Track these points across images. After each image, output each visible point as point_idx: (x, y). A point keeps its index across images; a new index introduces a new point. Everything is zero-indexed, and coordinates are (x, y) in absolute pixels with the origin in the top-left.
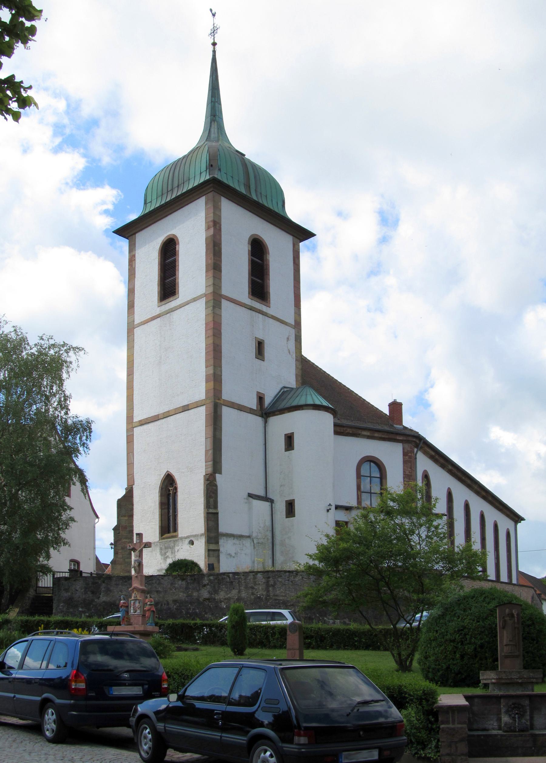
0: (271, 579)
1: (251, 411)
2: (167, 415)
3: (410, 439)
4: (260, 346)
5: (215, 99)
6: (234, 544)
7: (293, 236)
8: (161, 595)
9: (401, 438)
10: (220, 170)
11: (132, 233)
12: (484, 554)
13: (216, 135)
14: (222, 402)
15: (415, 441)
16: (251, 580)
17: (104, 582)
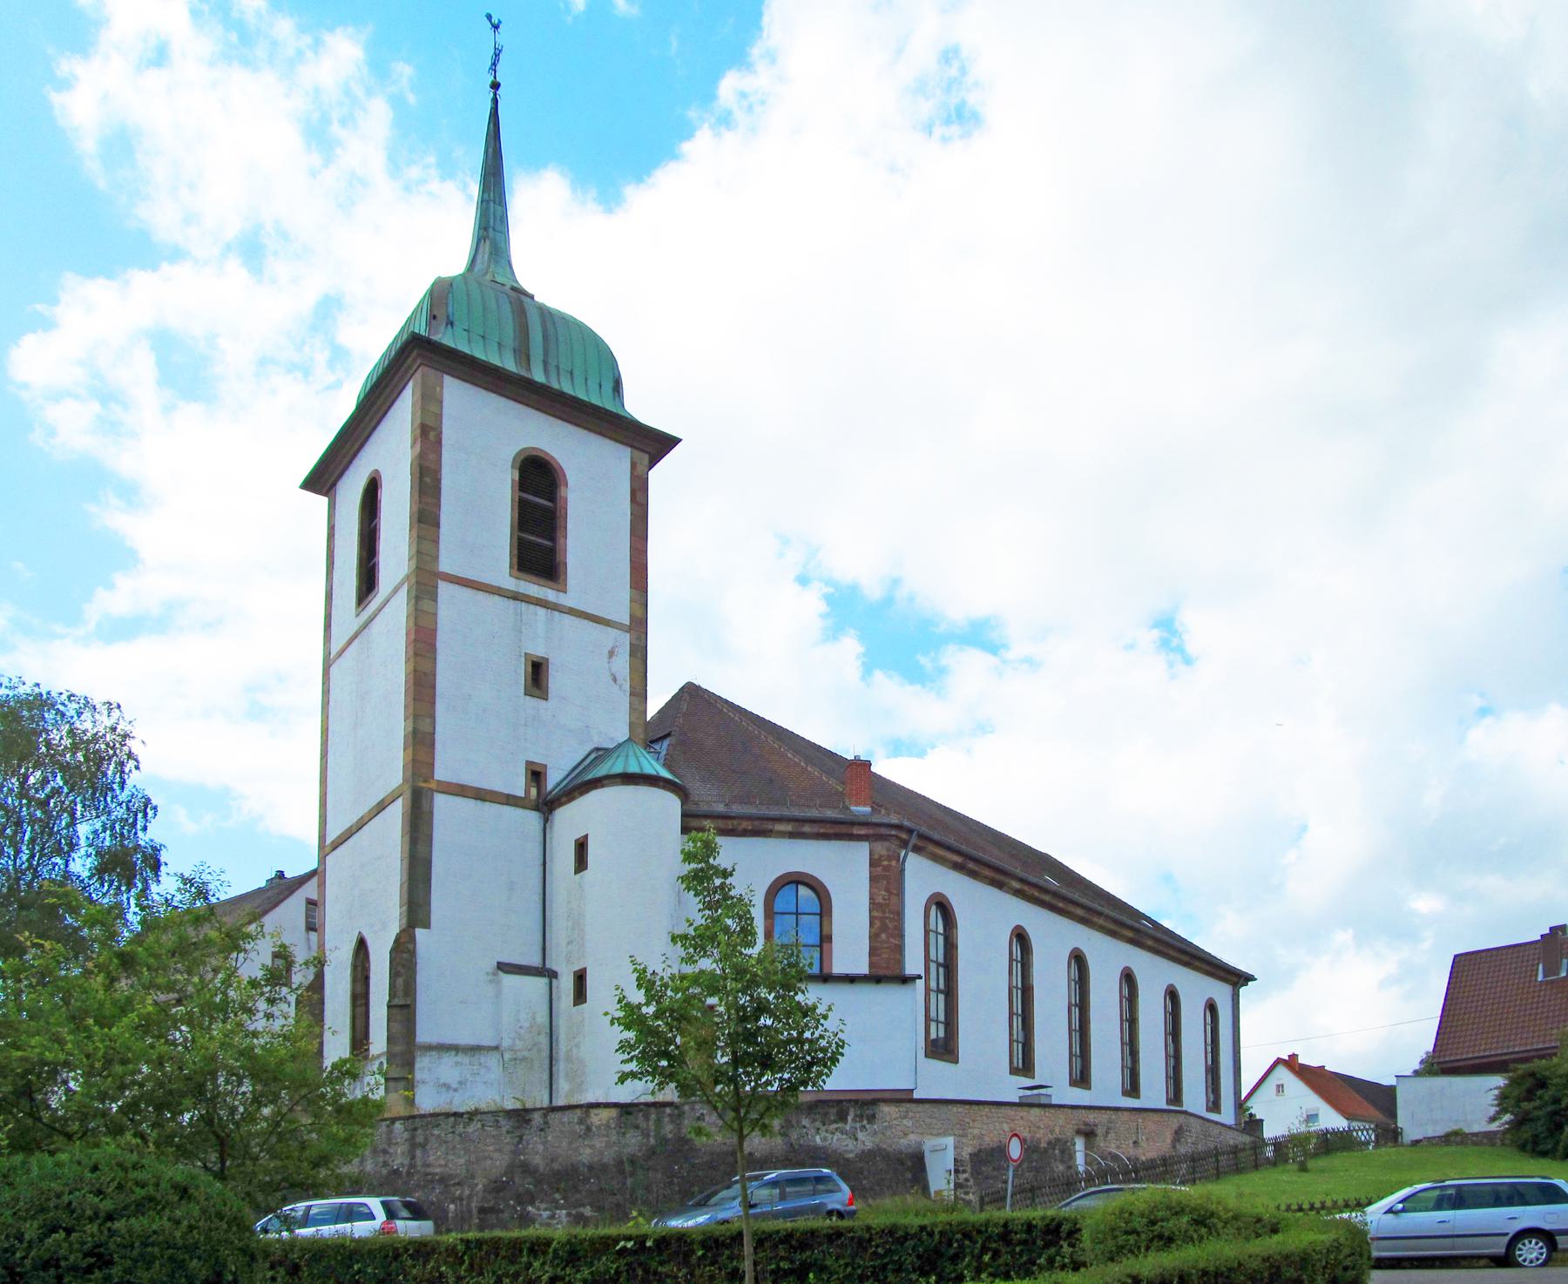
0: (419, 1131)
1: (509, 800)
2: (360, 825)
3: (883, 831)
4: (537, 674)
5: (489, 196)
6: (457, 1064)
7: (631, 446)
9: (863, 832)
10: (451, 323)
14: (433, 785)
15: (897, 836)
16: (384, 1136)
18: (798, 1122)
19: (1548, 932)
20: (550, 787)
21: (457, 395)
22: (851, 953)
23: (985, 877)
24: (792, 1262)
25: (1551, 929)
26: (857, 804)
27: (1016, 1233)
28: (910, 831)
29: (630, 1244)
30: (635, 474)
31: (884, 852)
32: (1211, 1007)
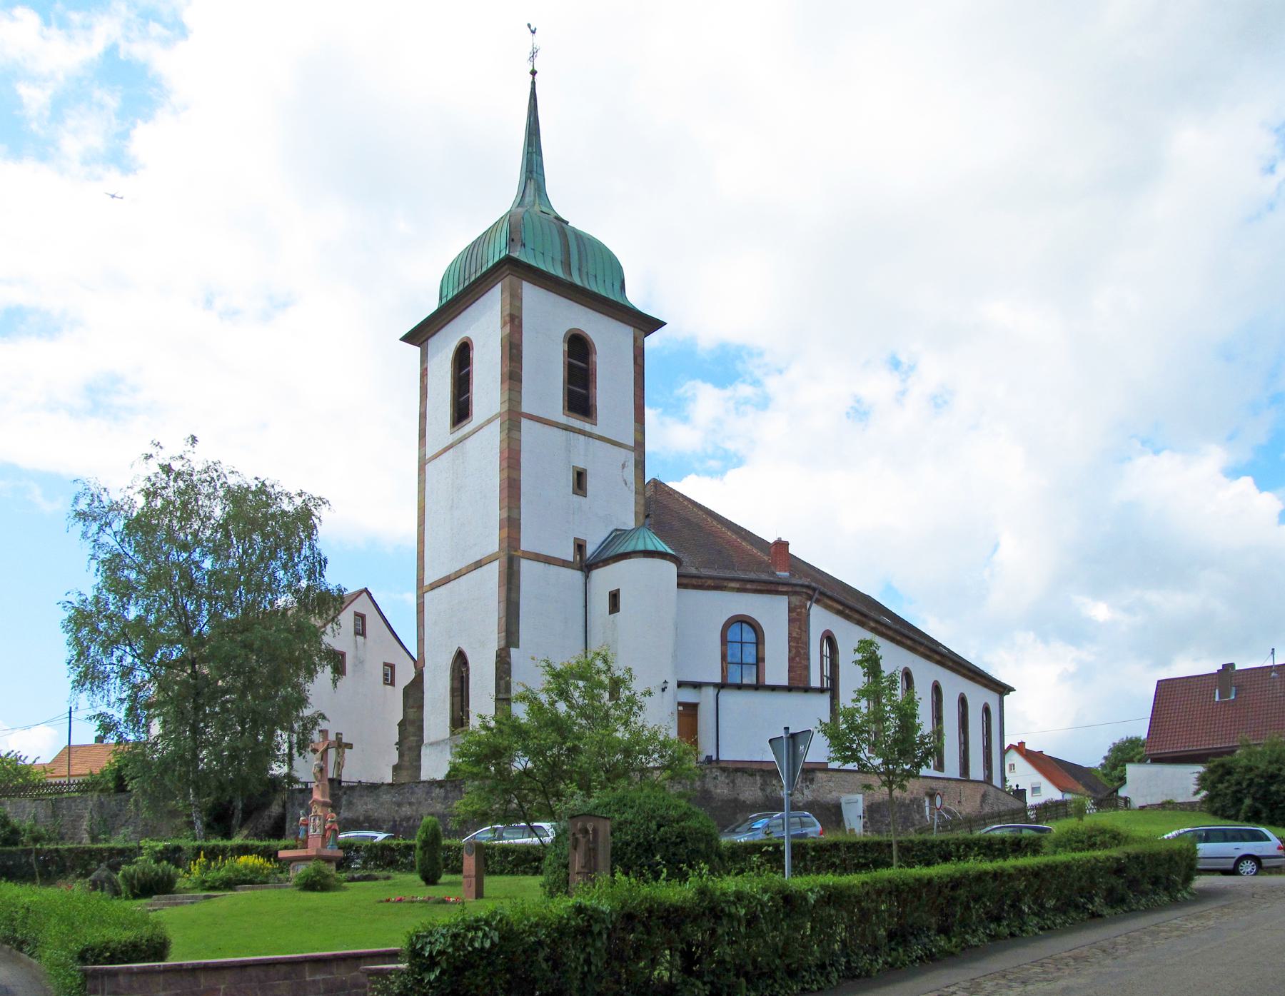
1: (564, 564)
2: (458, 575)
3: (798, 589)
4: (580, 479)
7: (634, 327)
8: (414, 808)
11: (424, 338)
12: (938, 733)
13: (532, 198)
15: (806, 593)
17: (345, 793)
18: (771, 782)
19: (1221, 668)
20: (588, 556)
21: (531, 294)
22: (777, 671)
23: (855, 619)
24: (866, 859)
25: (1223, 665)
26: (780, 571)
27: (995, 844)
28: (814, 590)
29: (770, 849)
30: (637, 345)
31: (797, 604)
32: (986, 710)
